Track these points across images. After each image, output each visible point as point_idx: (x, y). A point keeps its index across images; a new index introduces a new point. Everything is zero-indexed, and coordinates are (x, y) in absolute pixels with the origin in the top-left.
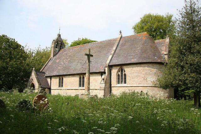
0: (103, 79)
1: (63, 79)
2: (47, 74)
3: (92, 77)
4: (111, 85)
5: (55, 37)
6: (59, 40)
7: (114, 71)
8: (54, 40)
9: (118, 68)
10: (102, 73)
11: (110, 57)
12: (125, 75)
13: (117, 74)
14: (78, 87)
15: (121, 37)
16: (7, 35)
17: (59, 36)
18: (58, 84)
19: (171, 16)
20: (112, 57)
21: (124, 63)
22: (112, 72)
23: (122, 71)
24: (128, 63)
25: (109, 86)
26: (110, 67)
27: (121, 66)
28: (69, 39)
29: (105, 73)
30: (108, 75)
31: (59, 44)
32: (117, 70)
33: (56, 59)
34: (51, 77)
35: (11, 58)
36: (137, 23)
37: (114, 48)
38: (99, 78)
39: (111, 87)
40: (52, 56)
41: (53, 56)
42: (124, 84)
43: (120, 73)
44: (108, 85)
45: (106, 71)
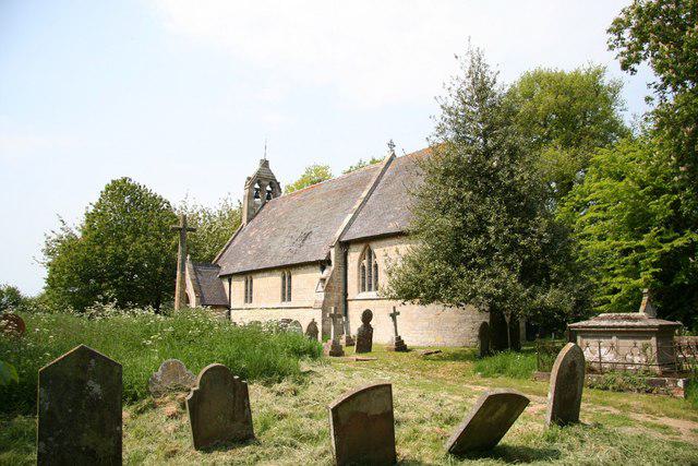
0: (323, 280)
1: (290, 277)
2: (224, 271)
3: (300, 276)
4: (346, 294)
5: (253, 169)
6: (265, 175)
7: (354, 256)
8: (249, 179)
9: (362, 247)
10: (323, 264)
11: (350, 216)
12: (376, 266)
13: (359, 264)
14: (279, 304)
15: (391, 160)
16: (125, 176)
17: (265, 164)
18: (243, 296)
19: (598, 73)
20: (353, 219)
21: (370, 235)
22: (349, 258)
23: (370, 257)
24: (379, 233)
25: (342, 298)
26: (344, 246)
27: (366, 241)
28: (286, 176)
29: (328, 262)
30: (337, 268)
31: (264, 186)
32: (358, 254)
33: (251, 229)
34: (229, 277)
35: (136, 233)
36: (452, 102)
37: (364, 194)
38: (315, 275)
39: (346, 302)
40: (244, 221)
41: (248, 221)
42: (370, 293)
43: (365, 262)
44: (337, 296)
45: (333, 259)
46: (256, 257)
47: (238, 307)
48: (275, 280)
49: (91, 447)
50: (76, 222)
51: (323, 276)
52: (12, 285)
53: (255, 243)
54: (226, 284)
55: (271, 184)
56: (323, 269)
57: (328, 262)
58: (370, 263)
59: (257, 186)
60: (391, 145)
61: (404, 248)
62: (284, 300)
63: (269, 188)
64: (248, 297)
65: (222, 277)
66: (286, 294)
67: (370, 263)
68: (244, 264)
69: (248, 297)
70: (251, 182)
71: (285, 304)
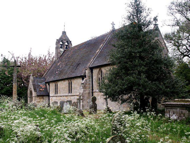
4: (93, 90)
5: (59, 35)
7: (95, 72)
8: (57, 40)
9: (98, 70)
10: (83, 77)
17: (64, 33)
25: (91, 91)
29: (85, 76)
38: (80, 81)
43: (100, 76)
46: (59, 74)
47: (53, 95)
48: (66, 83)
49: (33, 58)
50: (98, 36)
51: (83, 82)
52: (55, 41)
53: (59, 68)
54: (47, 85)
55: (67, 42)
56: (83, 79)
57: (85, 76)
58: (102, 76)
59: (61, 43)
60: (113, 24)
61: (111, 68)
62: (69, 93)
63: (66, 44)
64: (56, 92)
65: (46, 83)
66: (70, 90)
67: (102, 76)
68: (54, 77)
69: (56, 92)
70: (58, 41)
71: (70, 94)
